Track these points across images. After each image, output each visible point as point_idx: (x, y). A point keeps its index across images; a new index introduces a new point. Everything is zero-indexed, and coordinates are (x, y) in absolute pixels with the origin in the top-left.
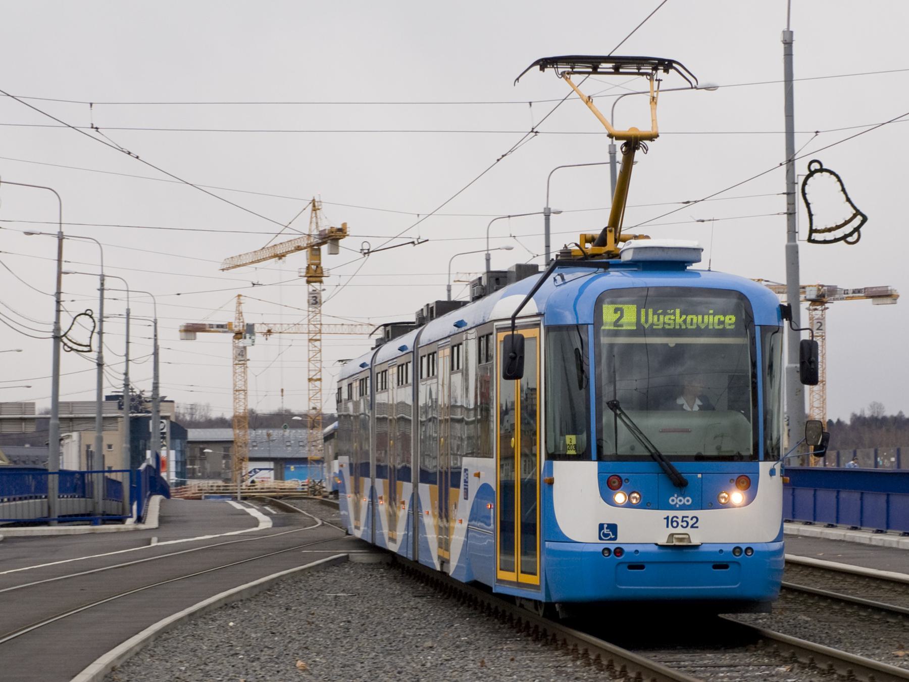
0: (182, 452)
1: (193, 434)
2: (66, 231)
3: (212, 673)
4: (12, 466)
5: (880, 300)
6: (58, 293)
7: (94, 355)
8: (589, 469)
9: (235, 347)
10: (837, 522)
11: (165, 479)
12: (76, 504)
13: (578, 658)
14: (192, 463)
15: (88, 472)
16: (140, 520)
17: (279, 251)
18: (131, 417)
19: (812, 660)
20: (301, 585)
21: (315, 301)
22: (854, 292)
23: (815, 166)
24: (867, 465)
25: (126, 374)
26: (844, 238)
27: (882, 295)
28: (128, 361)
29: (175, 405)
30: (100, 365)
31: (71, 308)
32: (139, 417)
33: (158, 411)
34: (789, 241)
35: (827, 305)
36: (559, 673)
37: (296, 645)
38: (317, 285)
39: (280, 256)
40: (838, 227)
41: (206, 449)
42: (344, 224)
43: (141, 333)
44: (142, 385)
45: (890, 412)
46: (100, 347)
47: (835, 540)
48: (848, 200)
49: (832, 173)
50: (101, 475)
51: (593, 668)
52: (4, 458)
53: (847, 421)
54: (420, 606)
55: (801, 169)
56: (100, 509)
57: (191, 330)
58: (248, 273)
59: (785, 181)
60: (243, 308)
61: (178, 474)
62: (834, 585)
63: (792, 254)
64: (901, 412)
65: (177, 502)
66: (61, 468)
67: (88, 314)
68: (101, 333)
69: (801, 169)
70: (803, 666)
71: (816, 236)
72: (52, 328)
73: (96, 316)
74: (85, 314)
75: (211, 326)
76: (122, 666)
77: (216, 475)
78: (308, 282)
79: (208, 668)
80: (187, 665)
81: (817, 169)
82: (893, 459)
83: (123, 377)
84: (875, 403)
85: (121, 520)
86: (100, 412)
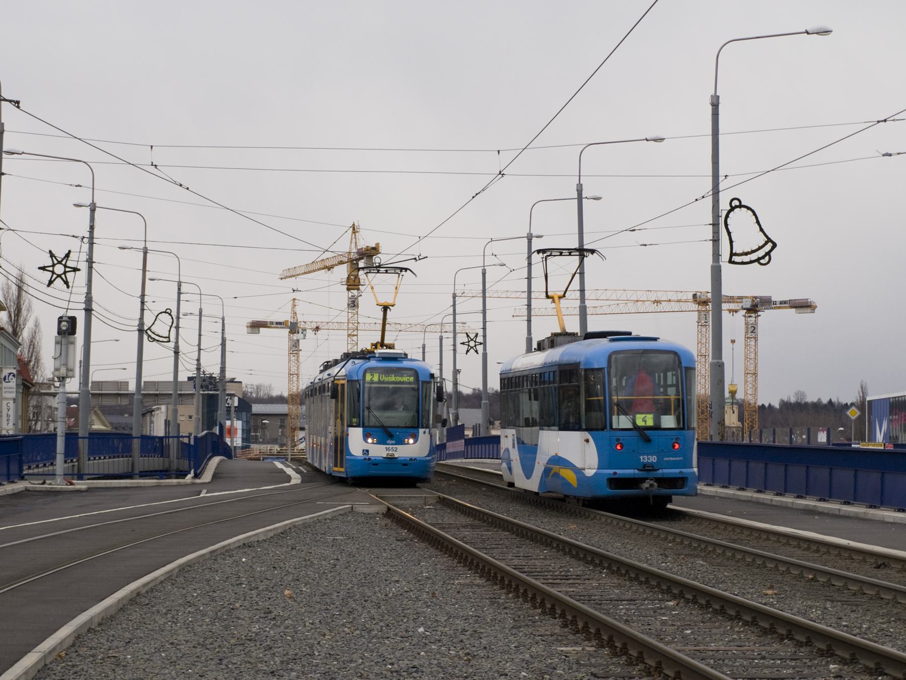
0: (247, 422)
1: (256, 408)
2: (149, 246)
3: (217, 599)
4: (114, 431)
5: (802, 310)
6: (143, 295)
7: (172, 345)
8: (359, 431)
9: (290, 339)
10: (747, 486)
11: (229, 444)
12: (155, 462)
13: (510, 592)
14: (256, 431)
15: (165, 437)
16: (197, 476)
17: (328, 264)
18: (203, 395)
19: (695, 597)
20: (309, 530)
21: (353, 304)
22: (781, 303)
23: (736, 203)
24: (782, 441)
25: (198, 360)
26: (758, 260)
27: (803, 306)
28: (200, 350)
29: (244, 385)
30: (177, 353)
31: (153, 307)
32: (211, 392)
33: (225, 390)
34: (714, 261)
35: (759, 313)
36: (492, 603)
37: (290, 578)
38: (355, 292)
39: (329, 268)
40: (753, 252)
41: (262, 418)
42: (378, 244)
43: (211, 329)
44: (211, 367)
45: (811, 398)
46: (177, 338)
47: (744, 501)
48: (761, 230)
49: (748, 208)
50: (176, 439)
51: (521, 600)
52: (108, 424)
53: (777, 406)
54: (398, 548)
55: (724, 206)
56: (174, 466)
57: (256, 326)
58: (299, 282)
59: (711, 215)
60: (297, 309)
61: (244, 440)
62: (733, 537)
63: (716, 273)
64: (819, 399)
65: (238, 464)
66: (144, 433)
67: (168, 312)
68: (177, 328)
69: (724, 206)
70: (687, 601)
71: (735, 259)
72: (137, 323)
73: (174, 314)
74: (165, 312)
75: (272, 323)
76: (147, 592)
77: (274, 441)
78: (348, 289)
79: (215, 595)
80: (199, 592)
81: (736, 205)
82: (804, 437)
83: (196, 362)
84: (799, 392)
85: (182, 474)
86: (176, 390)
